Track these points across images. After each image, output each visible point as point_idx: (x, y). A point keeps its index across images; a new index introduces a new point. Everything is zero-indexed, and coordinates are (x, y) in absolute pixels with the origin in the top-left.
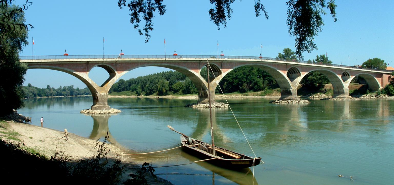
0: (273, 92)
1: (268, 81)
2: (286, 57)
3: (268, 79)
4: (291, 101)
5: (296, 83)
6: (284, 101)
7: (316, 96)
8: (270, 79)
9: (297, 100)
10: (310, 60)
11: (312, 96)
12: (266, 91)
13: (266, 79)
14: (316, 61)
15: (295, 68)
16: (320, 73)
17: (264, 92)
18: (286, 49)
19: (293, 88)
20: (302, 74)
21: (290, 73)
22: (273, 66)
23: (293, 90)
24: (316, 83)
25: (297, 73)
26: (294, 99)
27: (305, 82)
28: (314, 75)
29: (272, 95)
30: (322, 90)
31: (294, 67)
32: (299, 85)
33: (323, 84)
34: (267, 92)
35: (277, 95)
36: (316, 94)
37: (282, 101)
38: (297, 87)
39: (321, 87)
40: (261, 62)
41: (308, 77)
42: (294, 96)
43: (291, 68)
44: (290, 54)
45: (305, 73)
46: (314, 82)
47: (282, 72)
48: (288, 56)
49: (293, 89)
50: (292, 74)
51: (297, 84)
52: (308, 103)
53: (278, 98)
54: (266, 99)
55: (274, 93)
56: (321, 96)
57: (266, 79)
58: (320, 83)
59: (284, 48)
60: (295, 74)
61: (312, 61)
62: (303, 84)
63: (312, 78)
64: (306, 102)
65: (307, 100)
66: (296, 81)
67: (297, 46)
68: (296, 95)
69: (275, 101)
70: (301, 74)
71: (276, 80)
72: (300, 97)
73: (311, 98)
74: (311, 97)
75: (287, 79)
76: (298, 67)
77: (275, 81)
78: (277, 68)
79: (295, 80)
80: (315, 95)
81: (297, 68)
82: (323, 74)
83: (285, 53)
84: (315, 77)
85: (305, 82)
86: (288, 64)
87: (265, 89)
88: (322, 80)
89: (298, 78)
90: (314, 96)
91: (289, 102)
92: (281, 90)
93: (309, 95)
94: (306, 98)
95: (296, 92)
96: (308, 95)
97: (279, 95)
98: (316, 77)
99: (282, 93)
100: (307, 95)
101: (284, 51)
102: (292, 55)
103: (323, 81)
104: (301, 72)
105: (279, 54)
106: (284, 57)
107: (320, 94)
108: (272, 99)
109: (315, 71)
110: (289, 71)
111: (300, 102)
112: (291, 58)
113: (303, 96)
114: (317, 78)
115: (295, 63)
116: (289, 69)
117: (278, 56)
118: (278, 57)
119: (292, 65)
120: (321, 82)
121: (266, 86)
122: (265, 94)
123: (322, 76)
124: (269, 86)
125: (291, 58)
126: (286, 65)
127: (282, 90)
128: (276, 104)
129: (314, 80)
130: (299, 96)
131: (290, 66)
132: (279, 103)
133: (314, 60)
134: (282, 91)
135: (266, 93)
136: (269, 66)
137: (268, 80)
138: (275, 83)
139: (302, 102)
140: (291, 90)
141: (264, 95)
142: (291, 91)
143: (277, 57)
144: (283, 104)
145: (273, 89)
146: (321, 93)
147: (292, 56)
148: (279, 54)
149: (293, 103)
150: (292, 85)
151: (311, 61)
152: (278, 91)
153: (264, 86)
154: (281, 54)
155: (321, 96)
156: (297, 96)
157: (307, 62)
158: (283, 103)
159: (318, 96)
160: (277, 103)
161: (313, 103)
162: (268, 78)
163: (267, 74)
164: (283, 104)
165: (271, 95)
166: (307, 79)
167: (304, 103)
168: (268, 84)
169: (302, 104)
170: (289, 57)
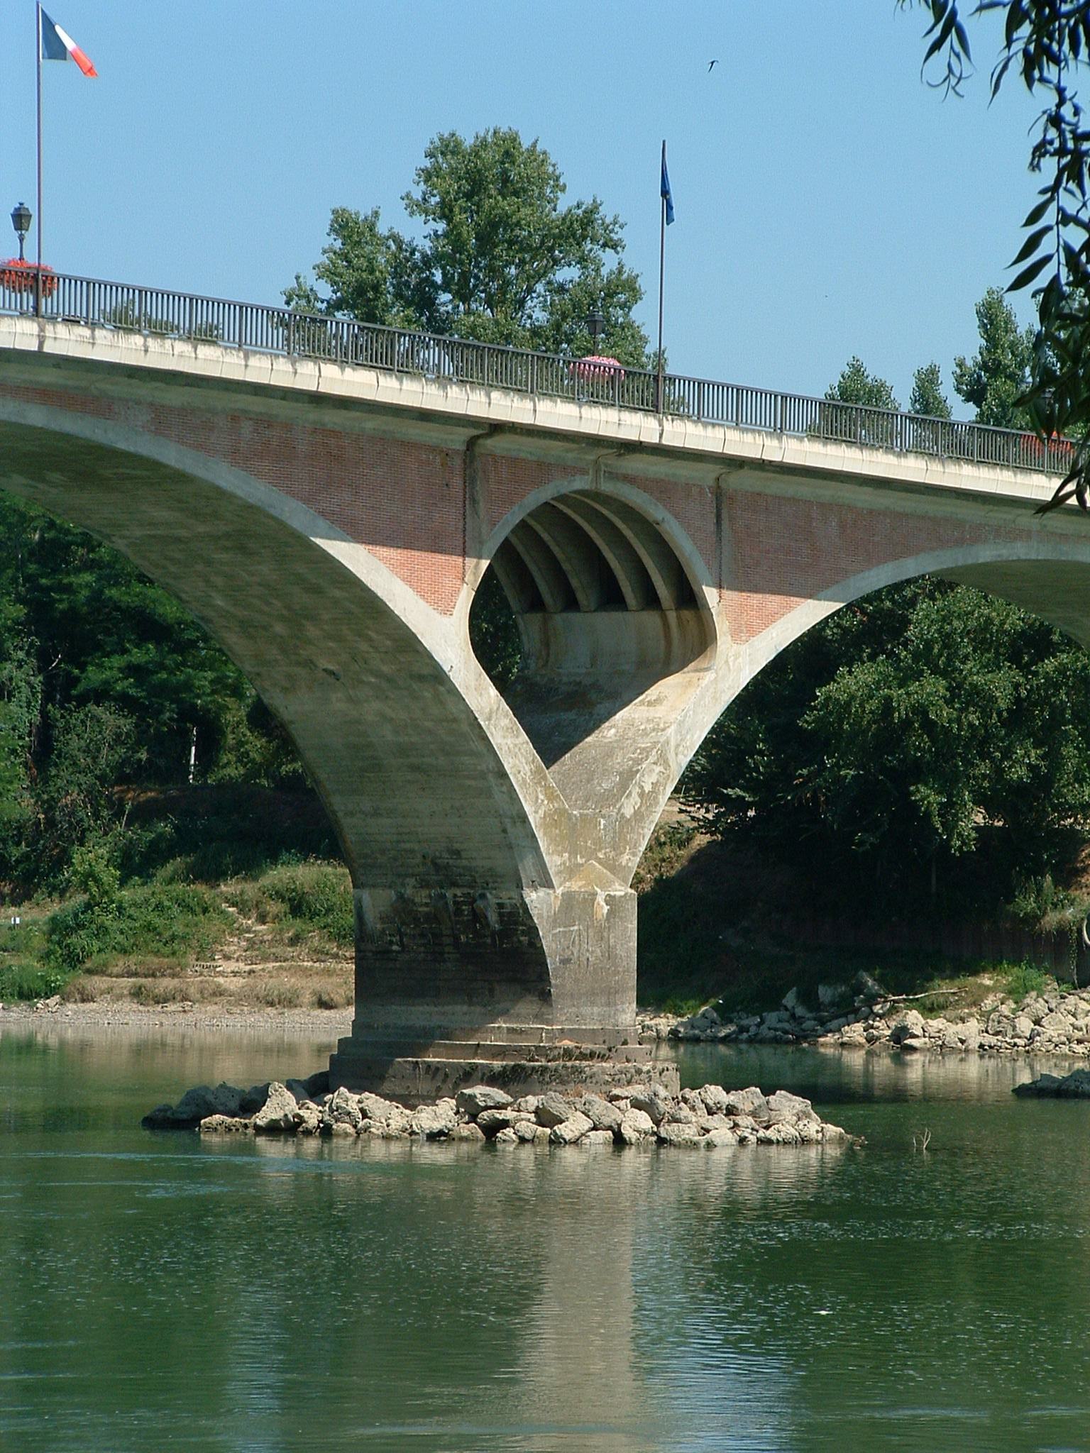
0: (212, 926)
1: (127, 724)
2: (464, 295)
3: (125, 685)
4: (532, 1101)
5: (628, 776)
6: (409, 1102)
7: (937, 1024)
8: (162, 690)
9: (638, 1091)
10: (874, 372)
11: (884, 1029)
12: (82, 898)
13: (94, 676)
14: (975, 394)
15: (607, 500)
16: (1016, 619)
17: (58, 928)
18: (468, 142)
19: (571, 871)
20: (736, 634)
21: (536, 604)
22: (236, 456)
23: (568, 897)
24: (948, 784)
25: (651, 600)
26: (598, 1066)
27: (760, 762)
28: (924, 655)
29: (192, 981)
30: (1051, 920)
31: (607, 487)
32: (664, 809)
33: (1072, 810)
34: (102, 931)
35: (289, 982)
36: (944, 989)
37: (372, 1101)
38: (631, 860)
39: (1039, 871)
40: (39, 358)
41: (828, 675)
42: (591, 1017)
43: (547, 509)
44: (535, 252)
45: (774, 601)
46: (917, 772)
47: (394, 568)
48: (494, 272)
49: (575, 885)
50: (559, 619)
51: (648, 798)
52: (813, 1153)
53: (286, 1050)
54: (84, 1047)
55: (234, 945)
56: (1025, 1025)
57: (94, 676)
58: (1020, 789)
59: (427, 137)
60: (606, 622)
61: (903, 398)
62: (738, 805)
63: (887, 707)
64: (787, 1130)
65: (800, 1103)
66: (622, 738)
67: (1042, 280)
68: (610, 995)
69: (251, 1102)
70: (722, 625)
71: (288, 707)
72: (675, 1038)
73: (855, 1059)
74: (855, 1032)
75: (473, 702)
76: (662, 489)
77: (262, 718)
78: (308, 500)
79: (609, 732)
80: (930, 1010)
81: (656, 512)
82: (1070, 643)
83: (441, 226)
84: (932, 687)
85: (760, 762)
86: (497, 428)
87: (84, 858)
88: (1048, 737)
89: (652, 693)
90: (914, 1019)
91: (492, 1129)
92: (366, 896)
93: (825, 993)
94: (769, 1057)
95: (610, 955)
96: (808, 998)
97: (308, 987)
98: (954, 692)
99: (385, 953)
100: (790, 999)
101: (427, 175)
102: (568, 274)
103: (1068, 750)
104: (710, 594)
105: (344, 225)
106: (423, 300)
107: (1017, 993)
108: (193, 1073)
109: (942, 584)
110: (506, 553)
111: (689, 1132)
112: (541, 316)
113: (725, 1014)
114: (978, 698)
115: (611, 415)
116: (514, 516)
117: (329, 273)
118: (325, 291)
119: (570, 454)
120: (1042, 782)
121: (85, 813)
122: (73, 960)
123: (1049, 665)
124: (143, 815)
125: (541, 316)
126: (472, 443)
127: (376, 902)
128: (272, 1149)
129: (919, 744)
130: (665, 1023)
131: (543, 470)
132: (326, 1132)
133: (928, 380)
134: (371, 916)
135: (78, 940)
136: (171, 454)
137: (126, 703)
138: (253, 773)
139: (721, 1132)
140: (534, 898)
141: (57, 978)
142: (533, 931)
143: (308, 296)
144: (396, 1148)
145: (211, 874)
146: (1036, 962)
147: (561, 289)
148: (344, 225)
149: (568, 1154)
150: (556, 819)
151: (877, 393)
152: (298, 906)
153: (49, 806)
154: (382, 229)
155: (1025, 1025)
156: (628, 1015)
157: (814, 414)
158: (387, 1138)
159: (973, 1025)
160: (288, 1129)
161: (900, 1148)
162: (132, 670)
163: (112, 592)
164: (396, 1148)
165: (166, 984)
166: (807, 721)
167: (747, 1154)
168: (126, 775)
169: (721, 1156)
170: (521, 303)
